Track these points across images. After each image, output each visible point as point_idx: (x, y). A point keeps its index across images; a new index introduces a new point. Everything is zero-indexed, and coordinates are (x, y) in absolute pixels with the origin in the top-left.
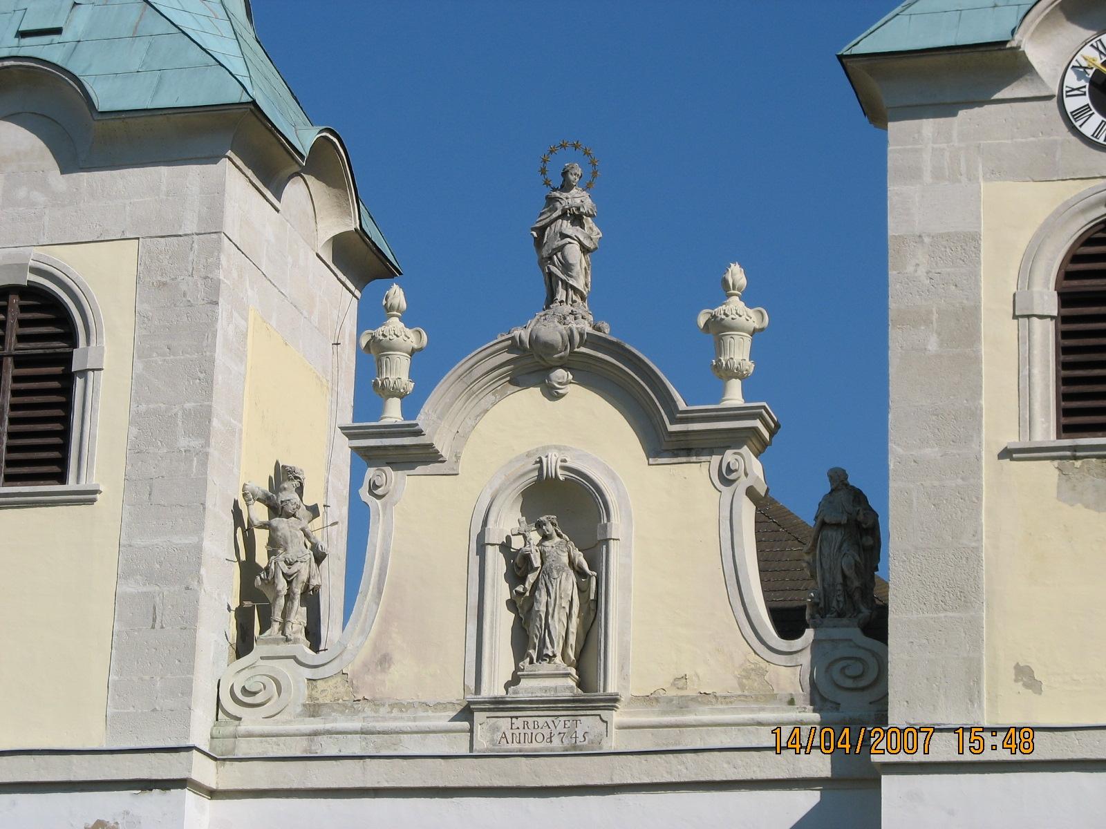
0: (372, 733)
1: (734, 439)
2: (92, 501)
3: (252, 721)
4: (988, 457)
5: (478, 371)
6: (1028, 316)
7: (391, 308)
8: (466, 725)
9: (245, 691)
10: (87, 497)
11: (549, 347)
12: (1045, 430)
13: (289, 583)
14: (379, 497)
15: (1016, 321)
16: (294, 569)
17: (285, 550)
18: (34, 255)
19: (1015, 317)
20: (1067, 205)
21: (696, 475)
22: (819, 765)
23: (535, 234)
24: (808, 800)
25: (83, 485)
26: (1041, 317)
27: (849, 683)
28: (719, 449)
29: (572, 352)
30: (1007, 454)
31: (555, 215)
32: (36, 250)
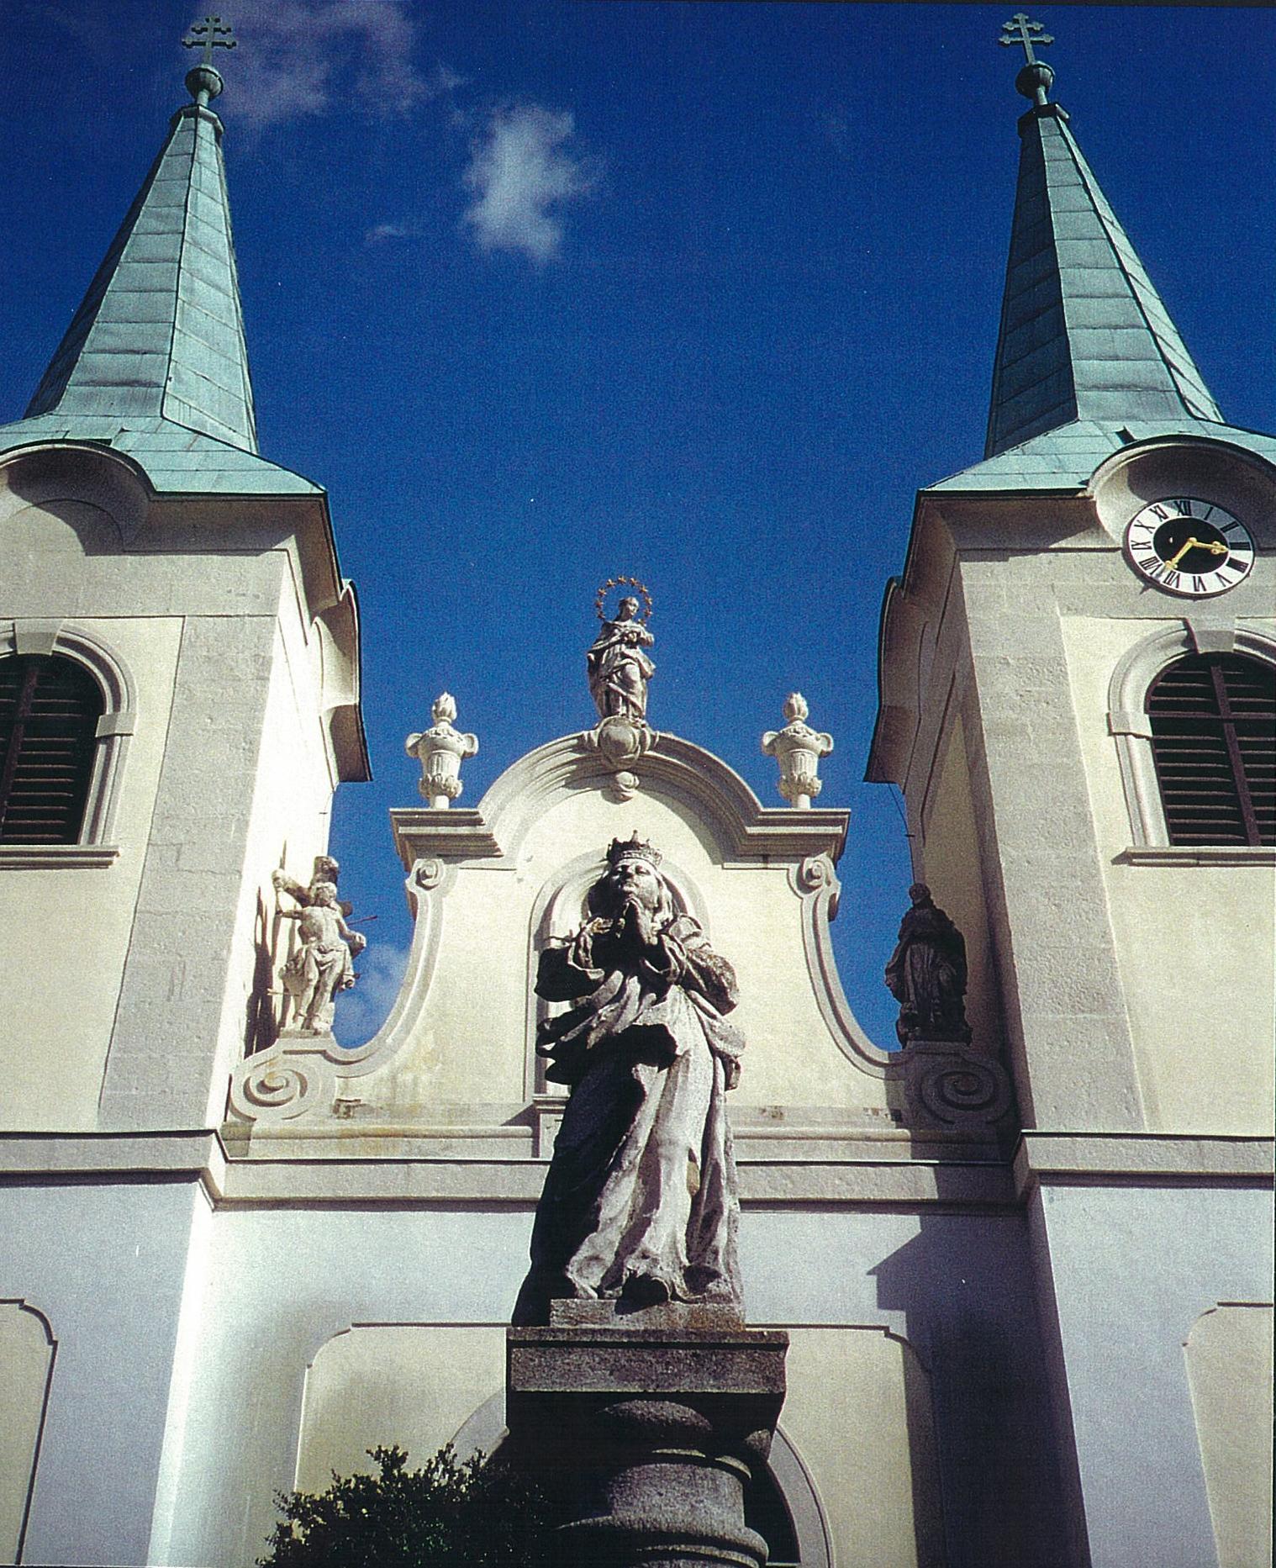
0: (416, 1136)
1: (811, 846)
2: (106, 864)
3: (265, 1121)
4: (1103, 863)
5: (541, 769)
6: (1126, 734)
7: (443, 713)
8: (528, 1129)
9: (262, 1086)
10: (102, 860)
11: (620, 747)
12: (1158, 837)
13: (321, 973)
14: (427, 888)
15: (1112, 739)
16: (328, 957)
17: (319, 938)
18: (65, 626)
19: (1111, 733)
20: (1159, 635)
21: (776, 880)
22: (924, 1183)
23: (592, 656)
24: (908, 1227)
25: (98, 845)
26: (1137, 736)
27: (935, 1104)
28: (799, 857)
29: (642, 756)
30: (1126, 858)
31: (614, 639)
32: (71, 623)
